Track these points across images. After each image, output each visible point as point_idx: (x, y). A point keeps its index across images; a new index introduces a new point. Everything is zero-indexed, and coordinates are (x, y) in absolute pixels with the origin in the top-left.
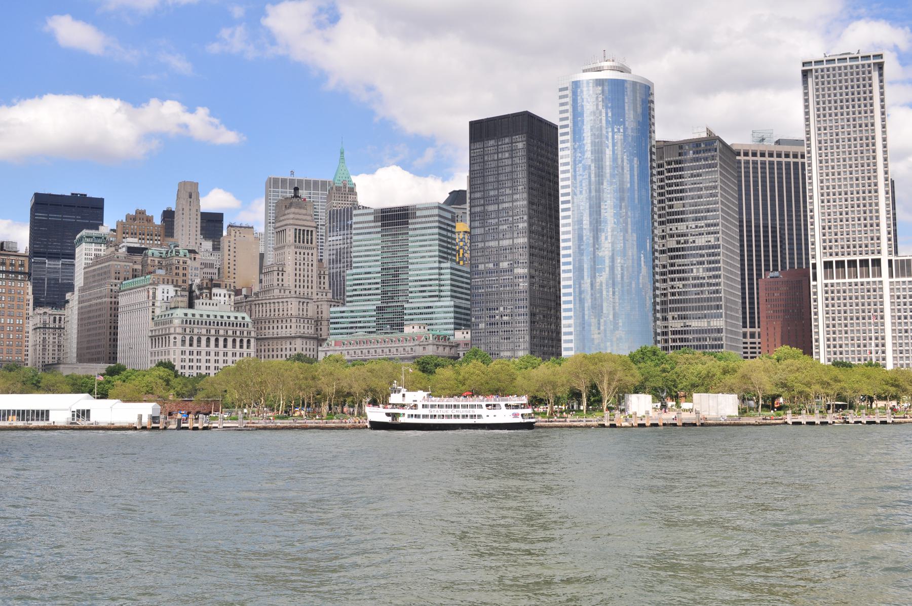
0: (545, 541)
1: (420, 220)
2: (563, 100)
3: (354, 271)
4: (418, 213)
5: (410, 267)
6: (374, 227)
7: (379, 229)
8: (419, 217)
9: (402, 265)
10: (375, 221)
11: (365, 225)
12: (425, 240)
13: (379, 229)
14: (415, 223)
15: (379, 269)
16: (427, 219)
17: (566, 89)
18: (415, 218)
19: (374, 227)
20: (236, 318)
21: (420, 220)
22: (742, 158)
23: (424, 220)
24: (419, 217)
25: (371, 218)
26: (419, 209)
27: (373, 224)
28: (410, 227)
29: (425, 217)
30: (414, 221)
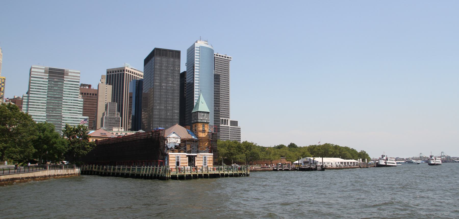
0: (217, 78)
1: (70, 77)
4: (69, 74)
5: (64, 98)
6: (45, 76)
7: (47, 80)
9: (59, 96)
12: (72, 87)
14: (68, 78)
18: (68, 76)
19: (45, 76)
21: (70, 77)
24: (70, 76)
25: (43, 71)
28: (65, 82)
29: (73, 76)
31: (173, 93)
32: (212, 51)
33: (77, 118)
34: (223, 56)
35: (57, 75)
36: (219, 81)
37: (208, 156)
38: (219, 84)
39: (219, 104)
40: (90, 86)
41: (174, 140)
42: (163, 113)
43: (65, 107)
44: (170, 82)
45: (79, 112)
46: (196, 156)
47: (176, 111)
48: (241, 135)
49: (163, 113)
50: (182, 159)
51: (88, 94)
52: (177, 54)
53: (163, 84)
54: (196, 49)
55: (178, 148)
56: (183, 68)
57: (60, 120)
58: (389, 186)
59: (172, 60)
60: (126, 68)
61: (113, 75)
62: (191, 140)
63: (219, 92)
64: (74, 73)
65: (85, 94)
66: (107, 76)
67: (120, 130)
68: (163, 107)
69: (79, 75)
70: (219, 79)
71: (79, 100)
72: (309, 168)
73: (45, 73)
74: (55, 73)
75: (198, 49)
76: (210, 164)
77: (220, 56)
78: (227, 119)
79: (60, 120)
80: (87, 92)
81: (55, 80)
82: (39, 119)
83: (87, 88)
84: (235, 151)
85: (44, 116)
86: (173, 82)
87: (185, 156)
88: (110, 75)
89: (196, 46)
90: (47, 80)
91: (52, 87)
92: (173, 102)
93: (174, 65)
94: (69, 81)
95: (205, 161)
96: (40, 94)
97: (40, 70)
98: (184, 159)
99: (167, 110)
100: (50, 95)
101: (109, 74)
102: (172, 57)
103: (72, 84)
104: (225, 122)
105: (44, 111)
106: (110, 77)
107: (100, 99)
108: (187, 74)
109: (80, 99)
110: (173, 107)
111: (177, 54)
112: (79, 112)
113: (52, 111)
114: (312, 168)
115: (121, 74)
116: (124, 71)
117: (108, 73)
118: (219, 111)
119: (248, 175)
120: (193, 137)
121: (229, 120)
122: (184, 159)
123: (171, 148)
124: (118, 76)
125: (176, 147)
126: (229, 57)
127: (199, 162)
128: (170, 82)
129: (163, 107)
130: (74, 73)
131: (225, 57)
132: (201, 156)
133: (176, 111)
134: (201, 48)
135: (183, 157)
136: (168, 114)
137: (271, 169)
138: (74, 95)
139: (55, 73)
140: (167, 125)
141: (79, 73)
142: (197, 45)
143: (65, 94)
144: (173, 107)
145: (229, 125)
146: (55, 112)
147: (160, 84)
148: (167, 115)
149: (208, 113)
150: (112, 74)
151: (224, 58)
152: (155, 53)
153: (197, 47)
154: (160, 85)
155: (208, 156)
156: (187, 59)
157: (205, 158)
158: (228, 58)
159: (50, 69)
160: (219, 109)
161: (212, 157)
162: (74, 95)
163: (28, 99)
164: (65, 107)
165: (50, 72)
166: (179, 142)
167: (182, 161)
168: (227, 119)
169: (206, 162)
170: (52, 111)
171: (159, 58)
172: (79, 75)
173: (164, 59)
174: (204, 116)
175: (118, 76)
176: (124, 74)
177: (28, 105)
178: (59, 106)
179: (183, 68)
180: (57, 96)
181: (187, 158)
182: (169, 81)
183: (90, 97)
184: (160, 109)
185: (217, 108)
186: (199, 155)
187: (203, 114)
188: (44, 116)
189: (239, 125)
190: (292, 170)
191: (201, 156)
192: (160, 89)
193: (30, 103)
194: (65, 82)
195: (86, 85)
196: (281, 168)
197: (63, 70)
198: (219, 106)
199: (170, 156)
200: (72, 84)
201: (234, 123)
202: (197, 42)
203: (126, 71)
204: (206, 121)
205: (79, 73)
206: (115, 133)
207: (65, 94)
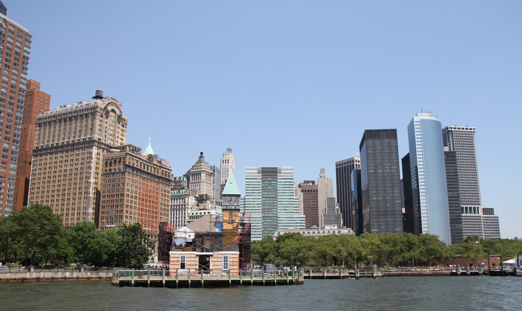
0: (450, 158)
1: (283, 175)
4: (282, 171)
5: (278, 197)
6: (258, 176)
7: (261, 180)
9: (274, 196)
18: (281, 173)
19: (258, 176)
20: (201, 213)
21: (283, 175)
25: (256, 171)
27: (257, 175)
28: (278, 180)
29: (286, 173)
31: (392, 180)
32: (439, 124)
33: (293, 218)
34: (463, 129)
35: (269, 174)
36: (455, 160)
37: (231, 256)
38: (456, 163)
39: (458, 188)
40: (313, 182)
41: (183, 235)
42: (381, 205)
43: (280, 207)
44: (387, 168)
45: (295, 211)
46: (212, 256)
47: (398, 202)
48: (500, 226)
49: (381, 205)
50: (189, 259)
51: (311, 191)
52: (392, 134)
53: (379, 171)
54: (415, 124)
55: (190, 245)
56: (403, 151)
57: (276, 221)
58: (196, 308)
59: (387, 141)
60: (356, 158)
61: (345, 167)
62: (208, 235)
63: (457, 173)
64: (287, 169)
65: (306, 191)
66: (337, 169)
67: (333, 228)
68: (381, 198)
69: (292, 171)
70: (455, 157)
71: (294, 197)
72: (500, 272)
73: (258, 173)
74: (268, 172)
75: (419, 123)
76: (235, 268)
77: (459, 128)
78: (476, 206)
79: (276, 221)
80: (310, 189)
81: (269, 179)
82: (256, 221)
83: (311, 184)
84: (403, 247)
85: (260, 218)
86: (390, 167)
87: (195, 256)
88: (340, 168)
89: (415, 120)
90: (261, 180)
91: (266, 187)
92: (393, 190)
93: (390, 147)
94: (282, 179)
95: (224, 263)
96: (255, 196)
97: (253, 169)
98: (193, 259)
99: (385, 201)
100: (264, 196)
101: (339, 167)
102: (387, 137)
103: (286, 182)
104: (475, 210)
105: (260, 213)
106: (340, 171)
107: (320, 195)
108: (410, 156)
109: (300, 196)
110: (393, 197)
111: (392, 134)
112: (295, 211)
113: (268, 212)
114: (505, 272)
115: (350, 165)
116: (353, 162)
117: (337, 166)
118: (459, 197)
119: (298, 283)
120: (217, 230)
121: (481, 208)
122: (193, 259)
123: (181, 245)
124: (348, 169)
125: (188, 244)
126: (473, 128)
127: (217, 263)
128: (387, 168)
129: (381, 198)
130: (287, 169)
131: (467, 129)
132: (219, 256)
133: (398, 202)
134: (423, 121)
135: (192, 258)
136: (388, 206)
137: (449, 272)
138: (289, 193)
139: (268, 172)
140: (387, 219)
141: (292, 169)
142: (416, 119)
143: (279, 193)
144: (393, 197)
145: (481, 214)
146: (270, 213)
147: (376, 170)
148: (386, 207)
149: (239, 196)
150: (341, 167)
151: (465, 130)
152: (366, 136)
153: (416, 122)
154: (376, 173)
155: (231, 256)
156: (409, 137)
157: (226, 258)
158: (471, 129)
159: (263, 168)
160: (458, 194)
161: (237, 256)
162: (289, 193)
163: (244, 202)
164: (280, 207)
165: (263, 172)
166: (193, 238)
167: (189, 263)
168: (476, 206)
169: (227, 264)
170: (268, 212)
171: (378, 140)
172: (292, 171)
173: (377, 142)
174: (231, 201)
175: (348, 169)
176: (353, 165)
177: (244, 207)
178: (275, 206)
179: (403, 151)
180: (271, 196)
181: (197, 259)
182: (386, 166)
183: (310, 191)
184: (377, 201)
185: (456, 193)
186: (215, 254)
187: (229, 198)
188: (260, 218)
189: (496, 213)
190: (484, 274)
191: (219, 256)
192: (376, 177)
193: (246, 206)
194: (278, 180)
195: (310, 182)
196: (464, 271)
197: (276, 168)
198: (458, 191)
199: (171, 256)
200: (286, 182)
201: (489, 211)
202: (417, 115)
203: (356, 161)
204: (233, 208)
205: (292, 169)
206: (326, 232)
207: (279, 193)
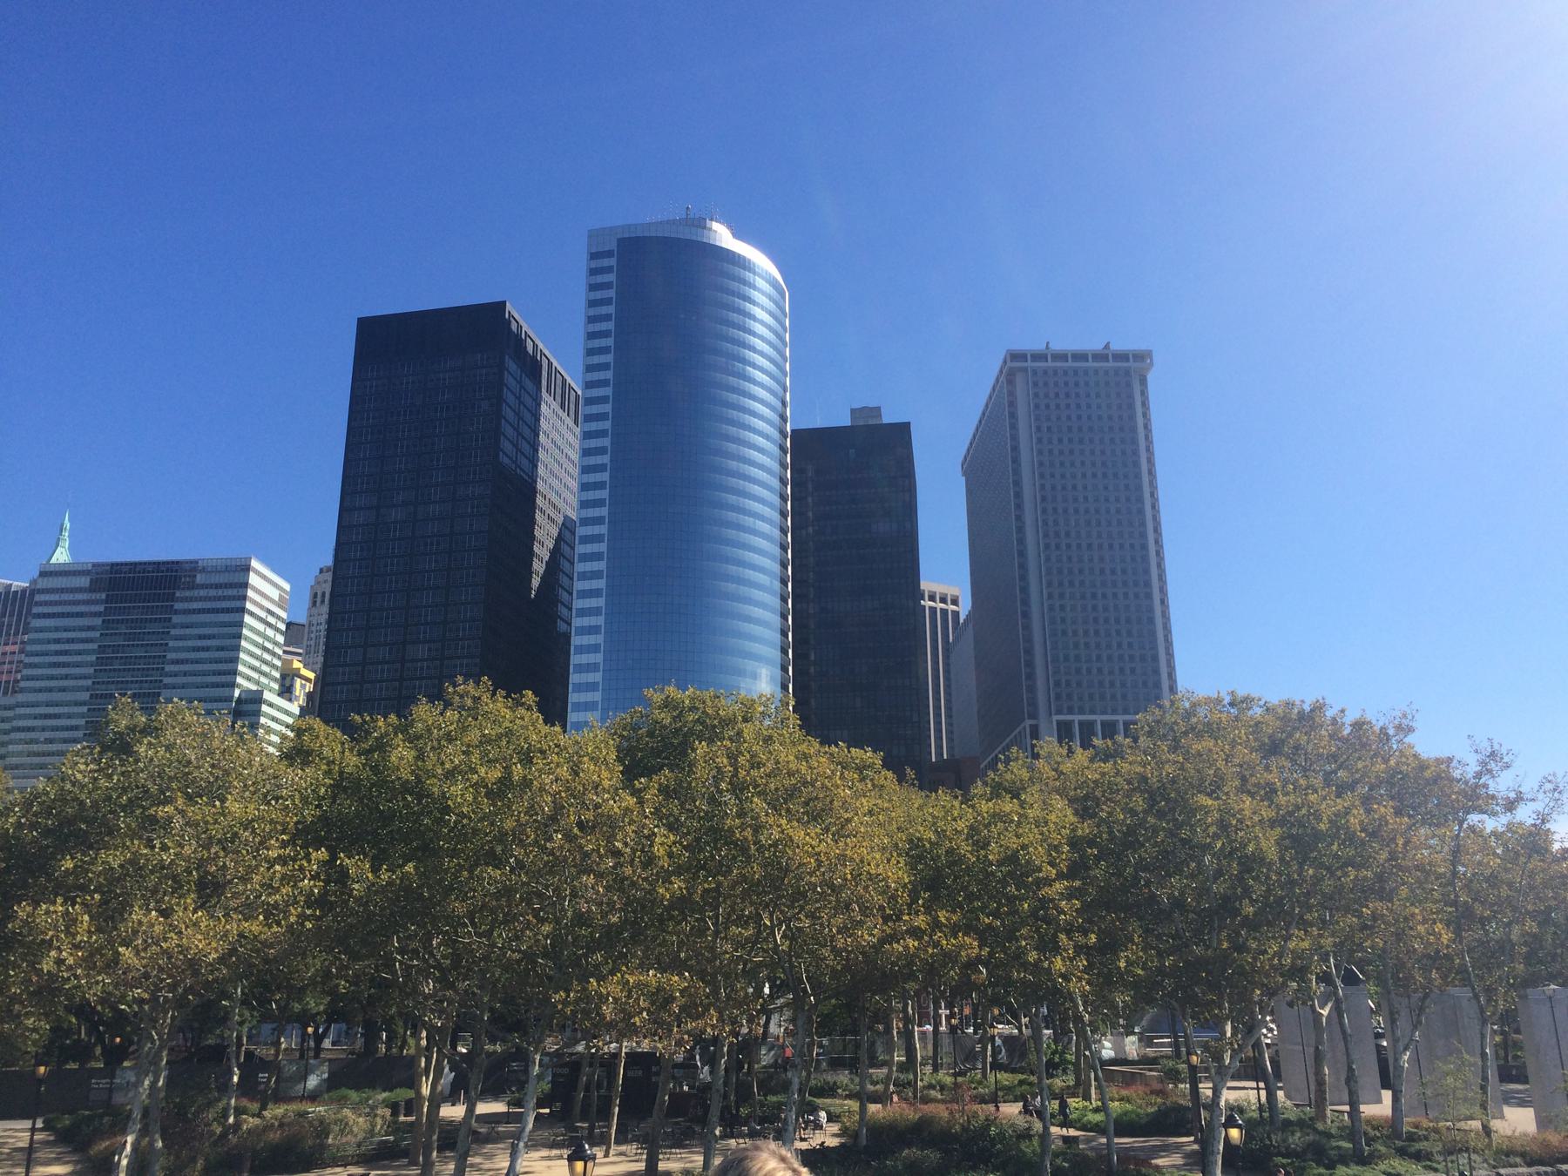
1: (202, 593)
2: (600, 279)
3: (20, 698)
4: (199, 579)
8: (203, 586)
10: (91, 590)
11: (66, 597)
13: (101, 608)
14: (190, 599)
15: (85, 696)
16: (66, 647)
17: (609, 254)
18: (193, 586)
21: (202, 593)
22: (927, 603)
23: (212, 593)
24: (203, 586)
26: (204, 570)
27: (85, 596)
30: (188, 594)
